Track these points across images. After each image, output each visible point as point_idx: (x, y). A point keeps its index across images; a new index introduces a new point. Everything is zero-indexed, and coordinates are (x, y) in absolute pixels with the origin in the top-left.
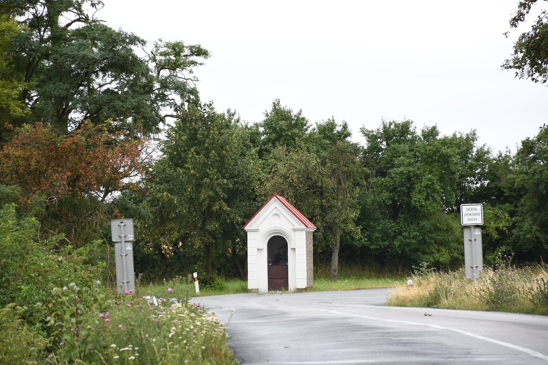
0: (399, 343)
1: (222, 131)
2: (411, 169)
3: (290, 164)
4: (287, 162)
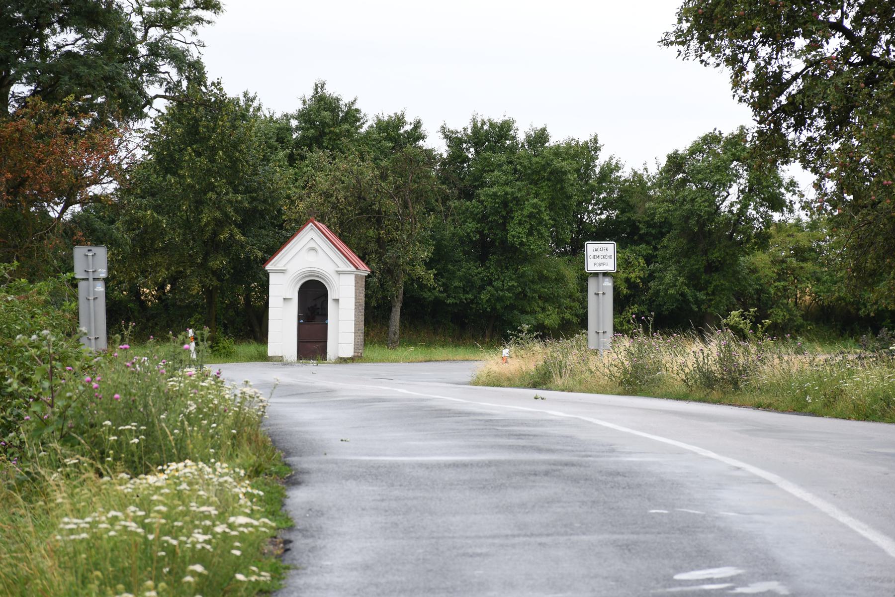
0: (510, 435)
1: (238, 123)
2: (508, 189)
3: (335, 176)
4: (327, 172)
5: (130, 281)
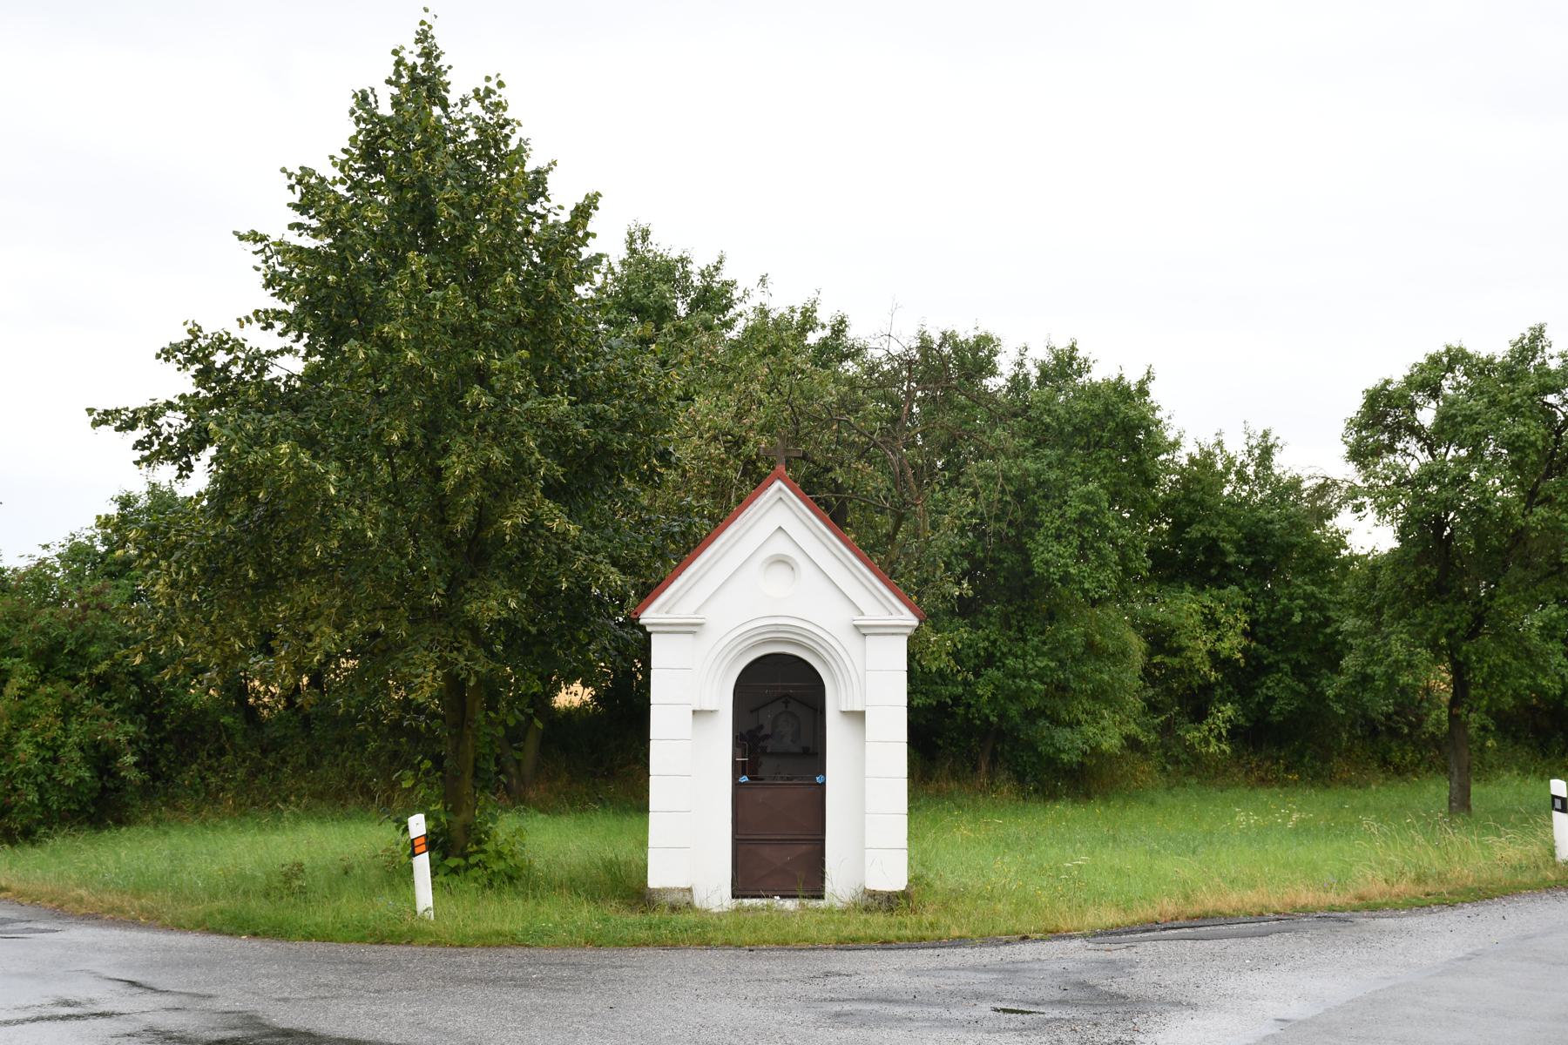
2: (1029, 464)
5: (223, 664)
